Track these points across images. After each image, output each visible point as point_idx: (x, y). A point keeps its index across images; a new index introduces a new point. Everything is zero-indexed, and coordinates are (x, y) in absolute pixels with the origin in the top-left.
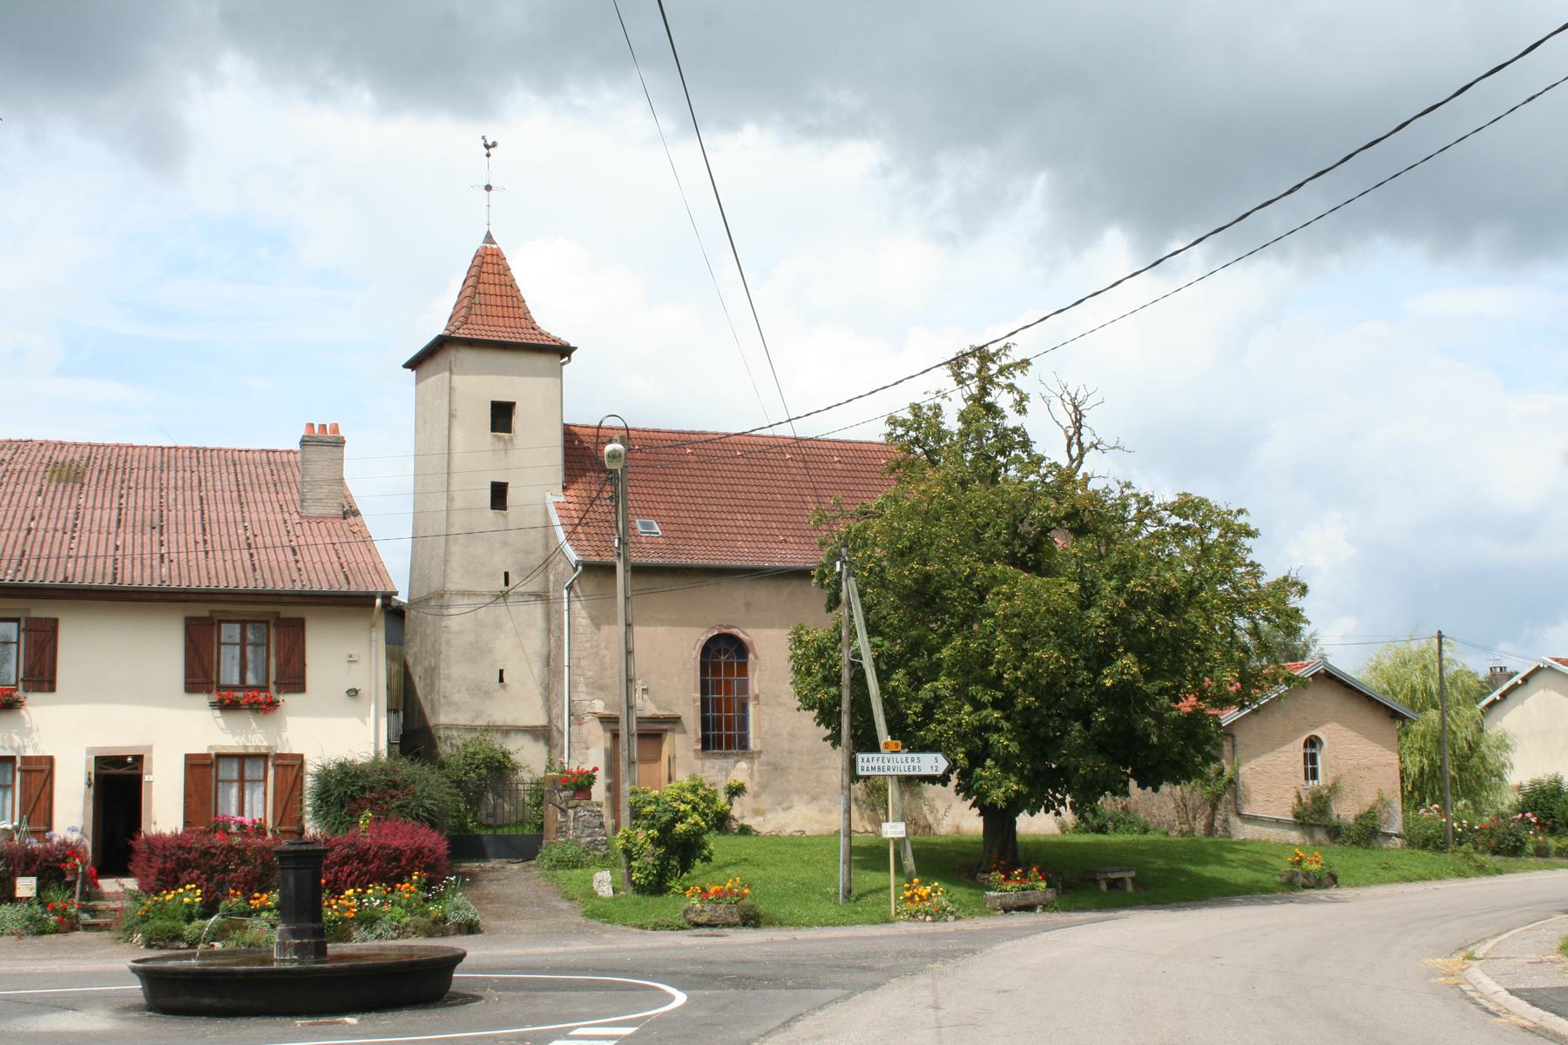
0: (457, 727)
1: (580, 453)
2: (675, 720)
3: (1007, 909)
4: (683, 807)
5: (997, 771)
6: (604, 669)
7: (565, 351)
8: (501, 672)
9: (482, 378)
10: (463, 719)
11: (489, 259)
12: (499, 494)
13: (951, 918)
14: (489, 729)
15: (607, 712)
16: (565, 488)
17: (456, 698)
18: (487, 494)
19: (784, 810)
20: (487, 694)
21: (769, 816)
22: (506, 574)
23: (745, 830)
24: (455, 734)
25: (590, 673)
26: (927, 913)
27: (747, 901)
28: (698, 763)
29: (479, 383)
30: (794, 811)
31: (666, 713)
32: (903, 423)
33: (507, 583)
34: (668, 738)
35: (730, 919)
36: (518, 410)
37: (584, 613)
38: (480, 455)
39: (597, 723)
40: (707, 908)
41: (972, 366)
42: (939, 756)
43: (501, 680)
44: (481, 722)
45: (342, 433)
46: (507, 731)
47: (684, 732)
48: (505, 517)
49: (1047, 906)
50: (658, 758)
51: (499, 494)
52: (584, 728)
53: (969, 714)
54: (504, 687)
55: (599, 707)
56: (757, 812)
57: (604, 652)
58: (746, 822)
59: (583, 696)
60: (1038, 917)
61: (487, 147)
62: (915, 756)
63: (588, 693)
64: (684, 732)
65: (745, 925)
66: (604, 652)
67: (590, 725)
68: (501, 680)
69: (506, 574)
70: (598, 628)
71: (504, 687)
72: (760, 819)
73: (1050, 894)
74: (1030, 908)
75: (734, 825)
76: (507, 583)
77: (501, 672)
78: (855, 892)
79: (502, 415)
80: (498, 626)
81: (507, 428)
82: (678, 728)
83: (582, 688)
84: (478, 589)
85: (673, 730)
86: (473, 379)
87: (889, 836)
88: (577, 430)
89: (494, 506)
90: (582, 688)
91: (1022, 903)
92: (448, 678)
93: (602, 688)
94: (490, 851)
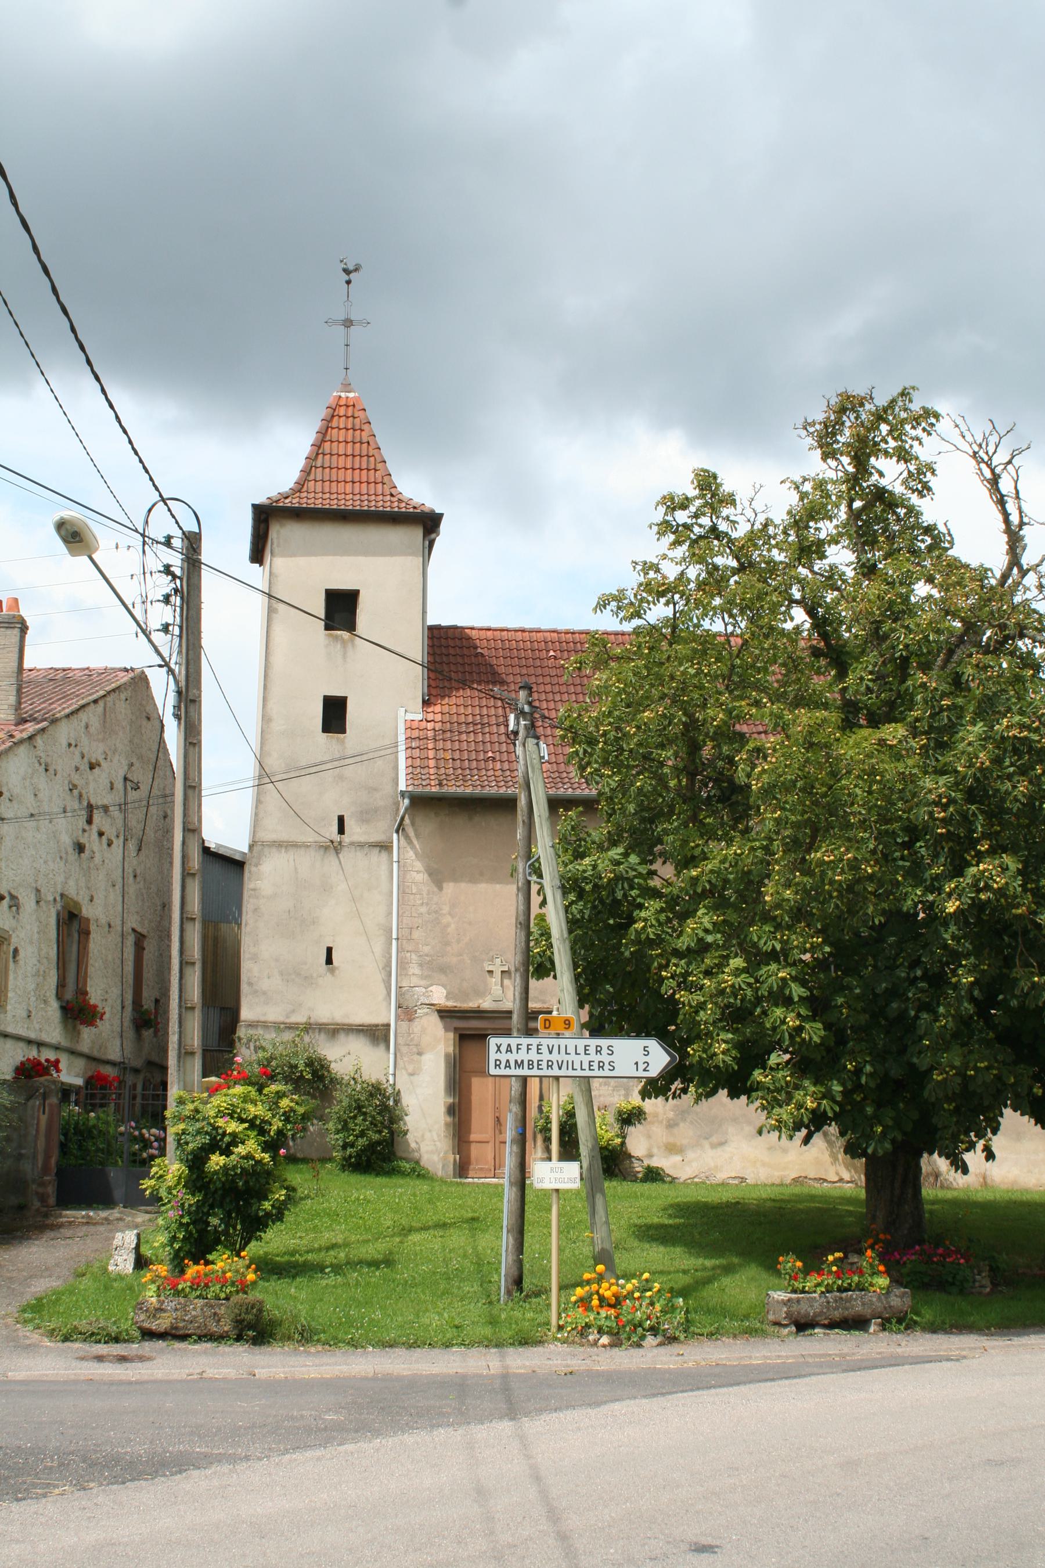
0: (265, 1025)
1: (454, 659)
3: (803, 1326)
4: (233, 1127)
5: (785, 1076)
6: (447, 944)
7: (429, 523)
8: (329, 951)
9: (314, 560)
10: (274, 1014)
11: (342, 411)
12: (334, 714)
13: (650, 1340)
14: (308, 1027)
15: (450, 1004)
16: (426, 703)
17: (265, 984)
18: (317, 712)
19: (713, 1146)
20: (309, 980)
21: (690, 1155)
22: (341, 820)
23: (653, 1175)
24: (260, 1031)
25: (426, 949)
26: (600, 1331)
27: (254, 1295)
29: (313, 566)
30: (728, 1149)
32: (685, 504)
33: (341, 830)
35: (214, 1328)
37: (419, 865)
38: (321, 666)
39: (435, 1018)
40: (170, 1305)
42: (653, 1044)
43: (329, 961)
44: (299, 1018)
45: (24, 612)
46: (334, 1031)
48: (343, 742)
49: (898, 1321)
51: (334, 714)
52: (416, 1026)
53: (737, 972)
54: (332, 972)
55: (439, 996)
56: (672, 1149)
57: (447, 919)
58: (655, 1163)
59: (415, 981)
60: (875, 1343)
61: (347, 271)
62: (604, 1042)
63: (423, 977)
65: (239, 1338)
66: (447, 919)
67: (424, 1021)
68: (329, 961)
69: (341, 820)
70: (441, 888)
71: (332, 972)
72: (678, 1158)
73: (900, 1299)
74: (856, 1323)
75: (638, 1167)
76: (341, 830)
77: (329, 951)
78: (526, 1284)
79: (341, 609)
80: (326, 888)
81: (350, 626)
83: (414, 969)
84: (301, 839)
86: (302, 561)
87: (548, 1185)
88: (474, 634)
89: (327, 728)
90: (414, 969)
91: (837, 1315)
92: (255, 958)
93: (443, 969)
94: (118, 1193)
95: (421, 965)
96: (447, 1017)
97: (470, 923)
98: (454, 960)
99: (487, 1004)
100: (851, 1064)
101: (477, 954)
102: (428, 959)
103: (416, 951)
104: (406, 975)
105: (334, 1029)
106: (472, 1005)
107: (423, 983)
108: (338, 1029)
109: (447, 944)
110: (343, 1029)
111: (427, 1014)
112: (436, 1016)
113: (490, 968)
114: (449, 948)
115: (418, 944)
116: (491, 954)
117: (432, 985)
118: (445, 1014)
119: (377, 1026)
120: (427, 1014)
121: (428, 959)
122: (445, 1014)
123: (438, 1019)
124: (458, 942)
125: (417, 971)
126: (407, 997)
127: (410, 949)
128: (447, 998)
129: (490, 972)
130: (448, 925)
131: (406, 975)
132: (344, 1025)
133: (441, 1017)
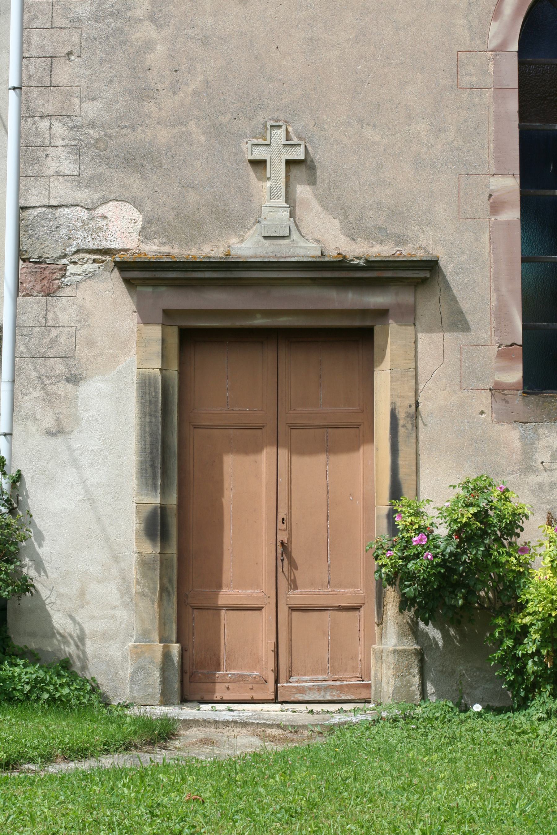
2: (423, 274)
6: (146, 94)
25: (91, 110)
28: (512, 436)
31: (382, 250)
34: (394, 340)
36: (390, 310)
39: (112, 285)
41: (471, 821)
47: (458, 322)
50: (359, 430)
52: (65, 309)
59: (61, 191)
63: (79, 181)
64: (458, 322)
66: (149, 30)
82: (428, 306)
85: (409, 315)
90: (60, 161)
93: (135, 160)
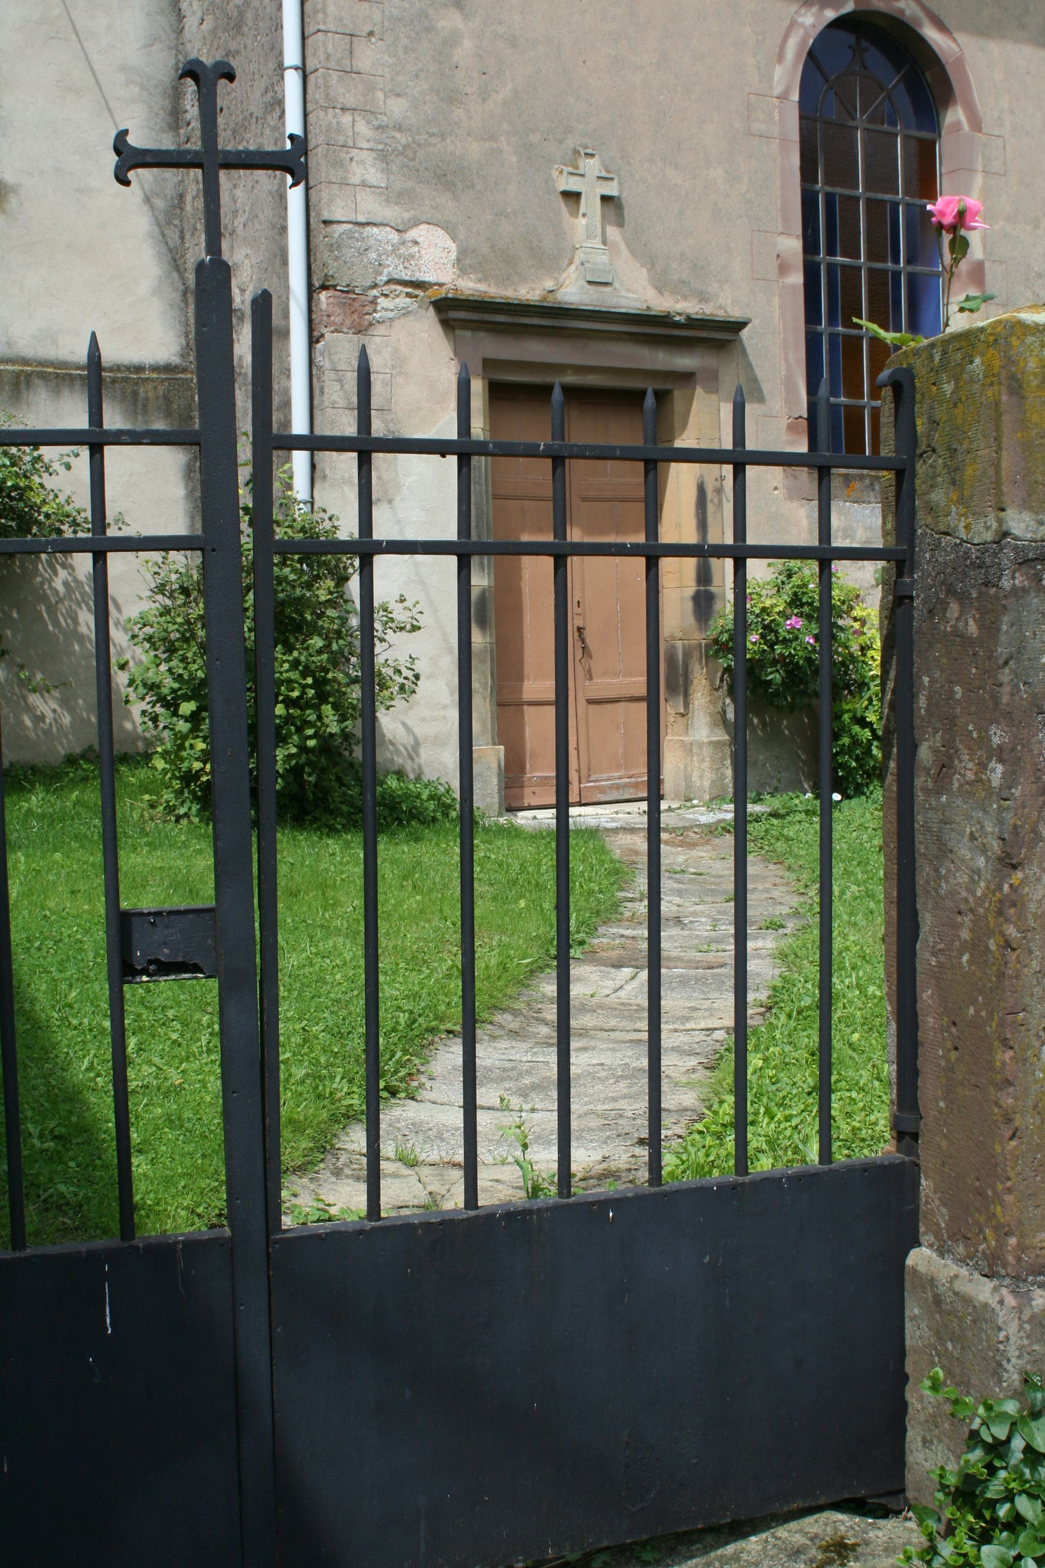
6: (453, 97)
15: (470, 286)
25: (397, 108)
39: (427, 327)
59: (369, 206)
93: (448, 177)
95: (383, 157)
96: (466, 324)
97: (513, 42)
98: (475, 149)
99: (572, 291)
100: (518, 1561)
101: (535, 138)
102: (402, 138)
103: (366, 111)
104: (344, 184)
105: (17, 375)
106: (528, 292)
107: (392, 213)
108: (29, 376)
109: (453, 97)
110: (44, 376)
111: (406, 313)
112: (430, 316)
113: (573, 185)
114: (459, 113)
115: (371, 88)
116: (571, 142)
117: (416, 223)
118: (456, 313)
119: (139, 369)
120: (406, 313)
121: (402, 138)
122: (456, 313)
123: (438, 330)
124: (484, 95)
125: (374, 175)
126: (349, 253)
127: (350, 101)
128: (462, 264)
129: (572, 197)
130: (453, 40)
131: (344, 184)
132: (42, 363)
133: (447, 324)
